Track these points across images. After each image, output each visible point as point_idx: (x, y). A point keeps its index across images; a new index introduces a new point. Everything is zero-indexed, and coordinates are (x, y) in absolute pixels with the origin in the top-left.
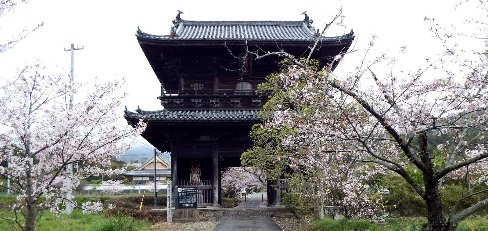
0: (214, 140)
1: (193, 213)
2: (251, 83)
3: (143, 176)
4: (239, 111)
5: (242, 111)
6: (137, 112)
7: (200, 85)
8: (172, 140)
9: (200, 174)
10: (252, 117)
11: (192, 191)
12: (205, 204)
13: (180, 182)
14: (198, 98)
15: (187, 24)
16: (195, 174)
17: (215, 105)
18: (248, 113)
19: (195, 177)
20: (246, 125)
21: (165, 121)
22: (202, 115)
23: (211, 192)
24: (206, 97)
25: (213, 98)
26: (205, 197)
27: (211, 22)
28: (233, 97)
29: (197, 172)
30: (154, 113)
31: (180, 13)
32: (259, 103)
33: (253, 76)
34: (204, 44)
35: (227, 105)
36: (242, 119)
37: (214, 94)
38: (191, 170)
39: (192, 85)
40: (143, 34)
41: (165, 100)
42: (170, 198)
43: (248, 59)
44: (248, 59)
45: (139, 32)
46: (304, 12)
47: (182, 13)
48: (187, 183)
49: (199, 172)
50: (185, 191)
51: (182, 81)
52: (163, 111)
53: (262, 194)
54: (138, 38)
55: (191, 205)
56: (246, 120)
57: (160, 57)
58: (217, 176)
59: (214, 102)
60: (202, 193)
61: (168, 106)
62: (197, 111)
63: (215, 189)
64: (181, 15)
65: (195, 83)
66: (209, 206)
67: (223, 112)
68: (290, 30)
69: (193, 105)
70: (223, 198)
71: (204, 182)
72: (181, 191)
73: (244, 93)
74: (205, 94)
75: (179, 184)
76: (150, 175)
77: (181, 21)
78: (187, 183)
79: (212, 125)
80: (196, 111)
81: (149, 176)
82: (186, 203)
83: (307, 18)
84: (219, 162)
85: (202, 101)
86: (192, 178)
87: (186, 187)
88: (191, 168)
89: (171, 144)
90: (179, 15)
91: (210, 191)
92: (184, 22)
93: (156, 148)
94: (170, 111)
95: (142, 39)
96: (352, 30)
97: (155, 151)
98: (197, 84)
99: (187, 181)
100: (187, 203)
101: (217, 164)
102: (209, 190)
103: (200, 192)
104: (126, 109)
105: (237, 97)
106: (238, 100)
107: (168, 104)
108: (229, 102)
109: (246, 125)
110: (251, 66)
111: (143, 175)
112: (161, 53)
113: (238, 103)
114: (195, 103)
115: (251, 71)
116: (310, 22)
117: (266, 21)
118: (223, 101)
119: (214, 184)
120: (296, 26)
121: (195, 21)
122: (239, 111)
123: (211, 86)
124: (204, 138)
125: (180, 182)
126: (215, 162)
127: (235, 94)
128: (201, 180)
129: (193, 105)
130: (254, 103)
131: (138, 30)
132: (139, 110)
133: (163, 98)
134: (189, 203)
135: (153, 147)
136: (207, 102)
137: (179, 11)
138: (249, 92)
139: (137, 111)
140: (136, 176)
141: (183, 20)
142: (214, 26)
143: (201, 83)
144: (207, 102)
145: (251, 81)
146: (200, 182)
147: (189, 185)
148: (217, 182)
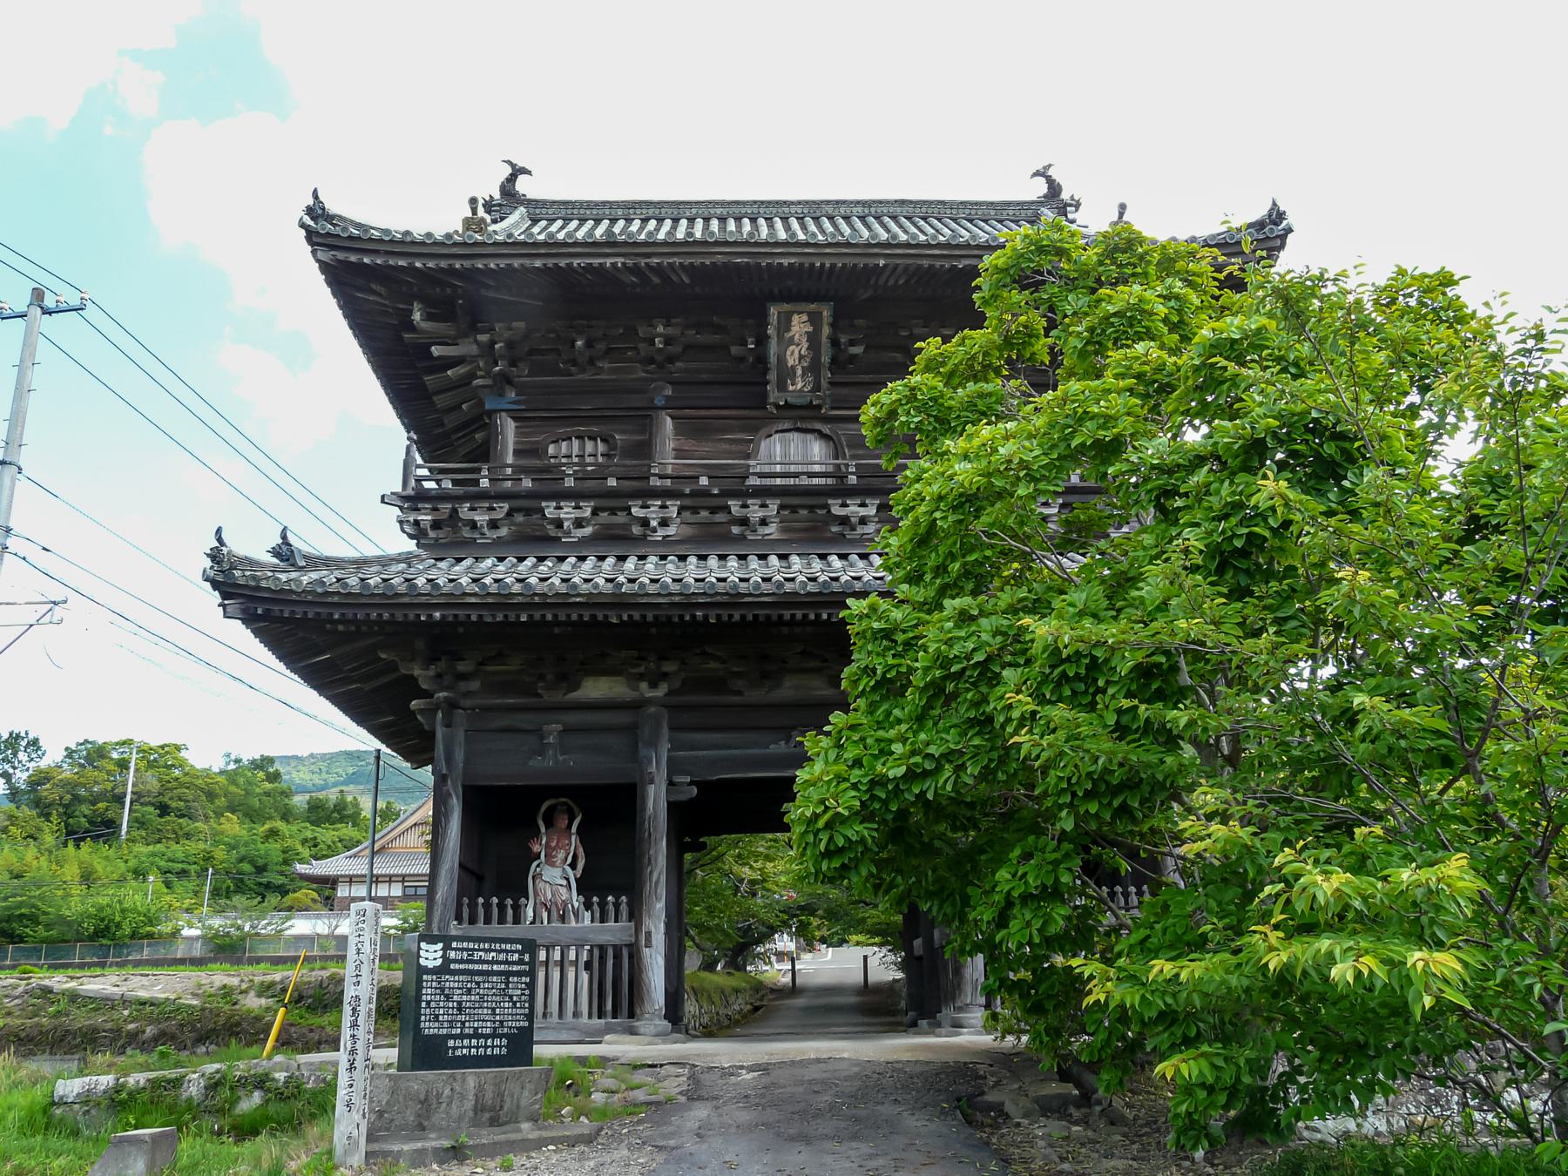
0: (650, 694)
1: (501, 1095)
2: (825, 437)
5: (783, 557)
6: (276, 561)
10: (836, 579)
11: (506, 962)
12: (596, 1021)
14: (575, 496)
15: (538, 210)
16: (553, 865)
17: (654, 530)
18: (817, 565)
19: (555, 876)
20: (805, 616)
22: (592, 574)
23: (631, 957)
26: (595, 986)
27: (649, 204)
28: (744, 494)
29: (561, 855)
30: (361, 563)
31: (517, 172)
32: (863, 521)
33: (833, 408)
34: (609, 262)
36: (788, 587)
37: (655, 482)
38: (536, 848)
39: (551, 450)
40: (330, 218)
41: (417, 509)
42: (363, 1010)
43: (811, 329)
44: (811, 329)
45: (316, 211)
46: (1040, 167)
48: (510, 912)
49: (575, 857)
50: (461, 961)
51: (509, 430)
52: (407, 559)
53: (865, 958)
54: (311, 236)
55: (498, 1047)
56: (810, 594)
57: (411, 327)
60: (581, 965)
61: (432, 534)
62: (572, 560)
63: (648, 945)
64: (521, 179)
66: (615, 1032)
67: (693, 560)
71: (596, 907)
73: (796, 475)
75: (466, 915)
76: (404, 876)
78: (510, 912)
81: (403, 878)
82: (462, 1036)
83: (1054, 189)
85: (595, 513)
86: (541, 885)
87: (469, 939)
88: (537, 834)
89: (440, 715)
90: (512, 179)
91: (625, 953)
92: (529, 203)
94: (442, 559)
97: (378, 758)
98: (576, 443)
99: (595, 899)
100: (470, 1037)
102: (617, 950)
103: (572, 955)
104: (220, 540)
105: (763, 493)
106: (764, 506)
107: (436, 525)
108: (720, 517)
109: (805, 616)
110: (825, 359)
114: (559, 523)
115: (824, 384)
117: (880, 202)
121: (581, 203)
122: (774, 560)
123: (644, 450)
124: (596, 689)
125: (473, 906)
127: (753, 481)
128: (582, 898)
129: (551, 530)
130: (844, 521)
131: (311, 202)
132: (285, 552)
133: (412, 499)
134: (486, 1037)
135: (363, 740)
136: (621, 518)
138: (817, 468)
139: (276, 552)
143: (594, 439)
148: (660, 906)
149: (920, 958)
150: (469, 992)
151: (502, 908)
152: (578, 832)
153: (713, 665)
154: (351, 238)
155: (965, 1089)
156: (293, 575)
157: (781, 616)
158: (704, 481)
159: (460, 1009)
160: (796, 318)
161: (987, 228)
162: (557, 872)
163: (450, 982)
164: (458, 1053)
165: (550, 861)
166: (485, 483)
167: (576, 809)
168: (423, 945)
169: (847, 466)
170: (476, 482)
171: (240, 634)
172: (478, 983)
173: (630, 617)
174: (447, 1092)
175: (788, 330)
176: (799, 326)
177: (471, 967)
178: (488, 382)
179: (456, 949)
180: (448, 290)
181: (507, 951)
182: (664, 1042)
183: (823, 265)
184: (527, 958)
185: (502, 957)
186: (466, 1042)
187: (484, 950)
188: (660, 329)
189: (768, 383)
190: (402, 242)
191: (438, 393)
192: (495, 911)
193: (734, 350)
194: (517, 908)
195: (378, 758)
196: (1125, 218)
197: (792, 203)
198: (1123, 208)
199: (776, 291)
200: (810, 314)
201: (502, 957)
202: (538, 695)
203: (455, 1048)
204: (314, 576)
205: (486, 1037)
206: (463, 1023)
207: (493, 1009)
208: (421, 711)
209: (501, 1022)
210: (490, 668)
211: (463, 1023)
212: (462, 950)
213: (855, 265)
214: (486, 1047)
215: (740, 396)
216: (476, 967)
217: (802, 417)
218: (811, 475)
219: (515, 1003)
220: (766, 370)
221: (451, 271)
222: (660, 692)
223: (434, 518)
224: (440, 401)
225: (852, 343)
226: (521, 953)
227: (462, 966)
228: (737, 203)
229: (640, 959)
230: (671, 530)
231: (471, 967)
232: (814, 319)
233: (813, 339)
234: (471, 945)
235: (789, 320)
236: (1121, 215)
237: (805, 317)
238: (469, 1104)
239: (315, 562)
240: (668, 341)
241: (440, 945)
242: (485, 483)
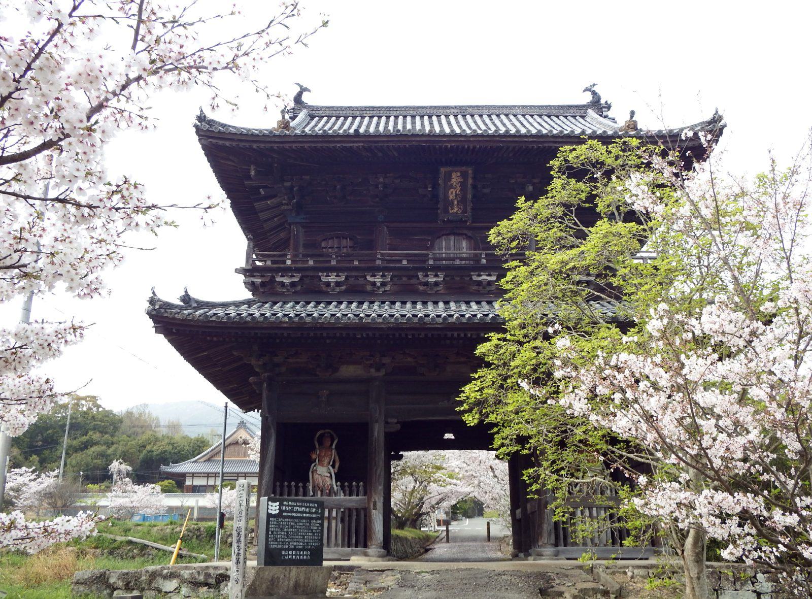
0: (377, 374)
2: (469, 238)
3: (208, 475)
4: (441, 304)
5: (446, 303)
6: (182, 304)
7: (344, 242)
8: (266, 375)
9: (337, 465)
11: (309, 513)
13: (282, 487)
15: (314, 113)
16: (323, 466)
17: (379, 288)
18: (464, 307)
19: (323, 473)
21: (251, 325)
23: (365, 516)
24: (356, 269)
25: (374, 270)
26: (346, 530)
27: (373, 108)
28: (425, 270)
29: (327, 461)
30: (225, 305)
33: (473, 222)
35: (407, 288)
38: (314, 456)
39: (323, 245)
40: (211, 123)
43: (462, 180)
44: (462, 180)
45: (201, 118)
46: (588, 85)
47: (307, 90)
48: (301, 489)
50: (288, 512)
52: (249, 303)
54: (198, 130)
55: (305, 555)
57: (249, 177)
58: (380, 471)
59: (378, 280)
60: (339, 519)
63: (375, 508)
65: (332, 238)
67: (398, 304)
68: (558, 122)
69: (325, 289)
70: (395, 532)
71: (347, 488)
72: (277, 512)
73: (454, 259)
74: (356, 263)
77: (305, 108)
79: (370, 334)
80: (332, 302)
82: (288, 550)
84: (388, 435)
86: (316, 476)
88: (314, 449)
90: (300, 95)
93: (228, 400)
95: (208, 134)
97: (226, 407)
100: (292, 550)
101: (382, 439)
103: (334, 514)
104: (154, 293)
105: (436, 269)
106: (436, 276)
107: (263, 284)
110: (469, 196)
111: (208, 473)
112: (252, 167)
113: (436, 284)
115: (469, 209)
116: (605, 107)
118: (400, 277)
119: (373, 493)
120: (572, 116)
122: (441, 304)
124: (348, 371)
125: (282, 487)
126: (376, 434)
128: (339, 483)
130: (479, 283)
132: (186, 299)
133: (249, 272)
134: (300, 550)
137: (301, 87)
140: (193, 475)
141: (310, 104)
142: (380, 117)
144: (361, 281)
145: (470, 234)
147: (305, 494)
148: (381, 488)
149: (520, 520)
150: (292, 527)
151: (297, 488)
152: (336, 448)
153: (409, 359)
154: (219, 132)
155: (541, 584)
156: (191, 311)
157: (446, 335)
158: (405, 262)
159: (287, 535)
160: (454, 175)
161: (558, 122)
163: (283, 522)
164: (287, 558)
165: (321, 463)
166: (289, 262)
167: (335, 436)
168: (270, 503)
169: (481, 254)
170: (284, 262)
171: (161, 340)
172: (296, 523)
173: (367, 335)
174: (282, 576)
176: (455, 179)
177: (293, 514)
178: (290, 207)
179: (285, 505)
180: (270, 160)
181: (310, 507)
182: (383, 561)
183: (469, 147)
184: (320, 511)
185: (307, 510)
186: (290, 552)
187: (299, 506)
188: (381, 180)
189: (438, 209)
190: (247, 135)
191: (262, 211)
192: (293, 488)
193: (421, 191)
194: (305, 488)
195: (226, 407)
196: (634, 119)
197: (452, 107)
198: (632, 114)
199: (444, 160)
200: (461, 172)
201: (307, 510)
203: (285, 555)
204: (202, 311)
205: (300, 550)
206: (289, 543)
207: (304, 536)
209: (307, 543)
210: (290, 360)
211: (289, 543)
212: (288, 506)
213: (486, 147)
214: (300, 555)
215: (427, 221)
216: (295, 515)
217: (456, 228)
218: (462, 259)
219: (314, 533)
220: (437, 202)
221: (272, 149)
222: (382, 373)
223: (261, 281)
224: (263, 216)
225: (484, 187)
226: (317, 508)
227: (289, 514)
228: (422, 107)
229: (370, 516)
230: (388, 288)
231: (293, 514)
232: (464, 175)
233: (463, 185)
234: (293, 504)
236: (632, 117)
237: (459, 174)
238: (292, 583)
239: (201, 305)
240: (385, 186)
241: (278, 503)
242: (289, 262)
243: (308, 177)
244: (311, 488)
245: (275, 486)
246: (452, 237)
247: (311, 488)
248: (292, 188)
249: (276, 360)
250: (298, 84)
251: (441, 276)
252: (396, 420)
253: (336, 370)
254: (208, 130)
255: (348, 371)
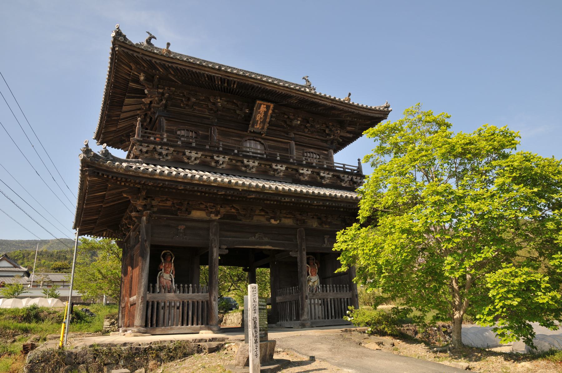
16: (167, 273)
33: (266, 135)
46: (305, 76)
71: (182, 288)
86: (162, 280)
90: (150, 39)
95: (122, 44)
96: (87, 145)
108: (239, 164)
110: (268, 120)
124: (197, 214)
128: (176, 285)
143: (192, 132)
146: (174, 287)
153: (233, 210)
160: (262, 106)
162: (168, 275)
175: (259, 109)
176: (263, 108)
188: (219, 100)
200: (267, 105)
202: (178, 215)
208: (135, 217)
232: (268, 107)
233: (266, 113)
235: (260, 106)
237: (265, 106)
243: (174, 89)
244: (158, 286)
245: (149, 287)
246: (252, 141)
247: (158, 286)
248: (163, 94)
249: (154, 203)
250: (148, 33)
251: (256, 164)
252: (226, 247)
253: (190, 213)
254: (123, 42)
255: (197, 214)
